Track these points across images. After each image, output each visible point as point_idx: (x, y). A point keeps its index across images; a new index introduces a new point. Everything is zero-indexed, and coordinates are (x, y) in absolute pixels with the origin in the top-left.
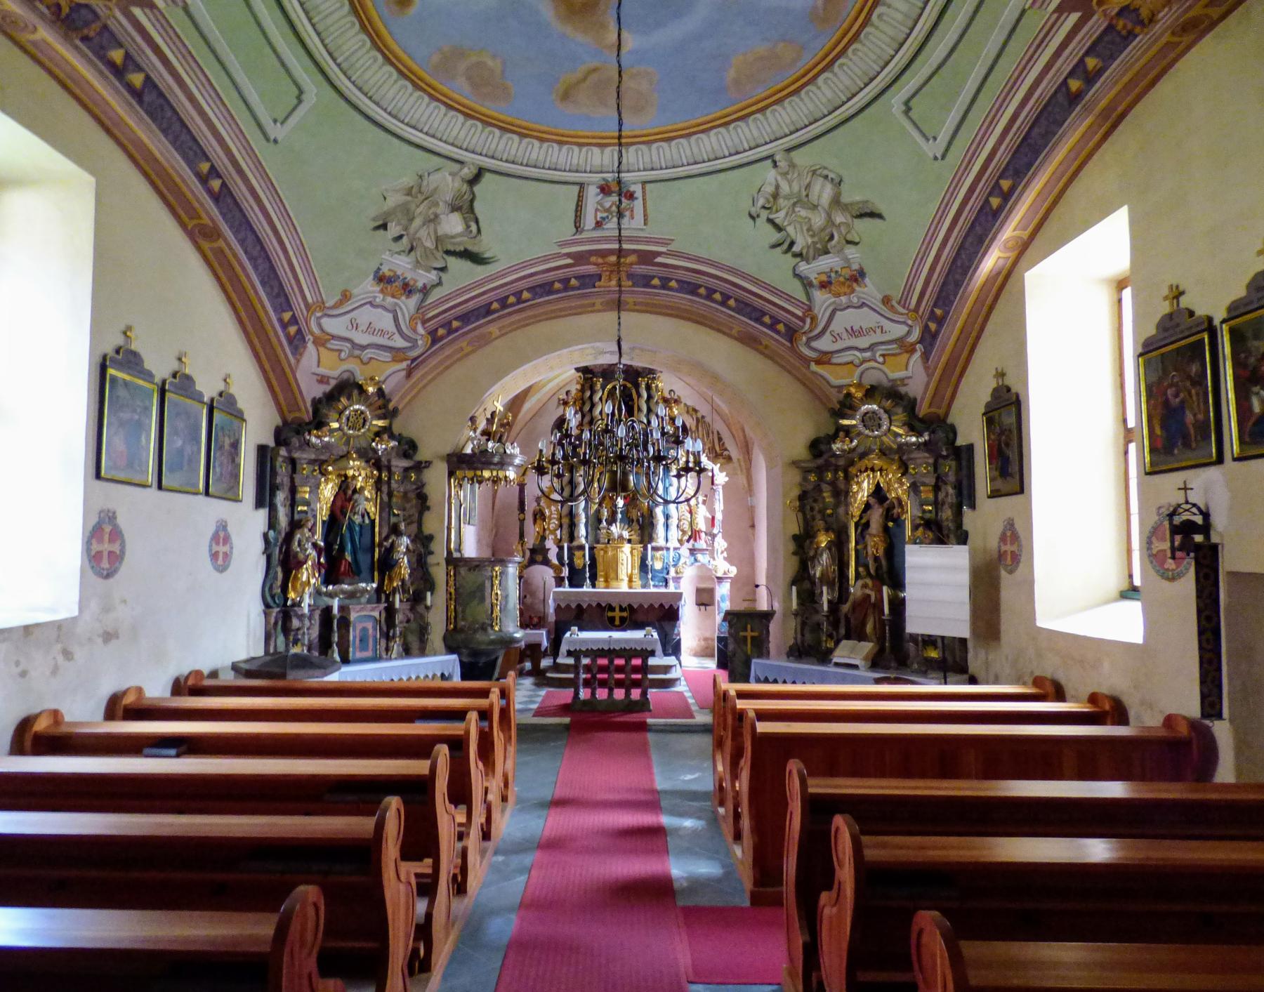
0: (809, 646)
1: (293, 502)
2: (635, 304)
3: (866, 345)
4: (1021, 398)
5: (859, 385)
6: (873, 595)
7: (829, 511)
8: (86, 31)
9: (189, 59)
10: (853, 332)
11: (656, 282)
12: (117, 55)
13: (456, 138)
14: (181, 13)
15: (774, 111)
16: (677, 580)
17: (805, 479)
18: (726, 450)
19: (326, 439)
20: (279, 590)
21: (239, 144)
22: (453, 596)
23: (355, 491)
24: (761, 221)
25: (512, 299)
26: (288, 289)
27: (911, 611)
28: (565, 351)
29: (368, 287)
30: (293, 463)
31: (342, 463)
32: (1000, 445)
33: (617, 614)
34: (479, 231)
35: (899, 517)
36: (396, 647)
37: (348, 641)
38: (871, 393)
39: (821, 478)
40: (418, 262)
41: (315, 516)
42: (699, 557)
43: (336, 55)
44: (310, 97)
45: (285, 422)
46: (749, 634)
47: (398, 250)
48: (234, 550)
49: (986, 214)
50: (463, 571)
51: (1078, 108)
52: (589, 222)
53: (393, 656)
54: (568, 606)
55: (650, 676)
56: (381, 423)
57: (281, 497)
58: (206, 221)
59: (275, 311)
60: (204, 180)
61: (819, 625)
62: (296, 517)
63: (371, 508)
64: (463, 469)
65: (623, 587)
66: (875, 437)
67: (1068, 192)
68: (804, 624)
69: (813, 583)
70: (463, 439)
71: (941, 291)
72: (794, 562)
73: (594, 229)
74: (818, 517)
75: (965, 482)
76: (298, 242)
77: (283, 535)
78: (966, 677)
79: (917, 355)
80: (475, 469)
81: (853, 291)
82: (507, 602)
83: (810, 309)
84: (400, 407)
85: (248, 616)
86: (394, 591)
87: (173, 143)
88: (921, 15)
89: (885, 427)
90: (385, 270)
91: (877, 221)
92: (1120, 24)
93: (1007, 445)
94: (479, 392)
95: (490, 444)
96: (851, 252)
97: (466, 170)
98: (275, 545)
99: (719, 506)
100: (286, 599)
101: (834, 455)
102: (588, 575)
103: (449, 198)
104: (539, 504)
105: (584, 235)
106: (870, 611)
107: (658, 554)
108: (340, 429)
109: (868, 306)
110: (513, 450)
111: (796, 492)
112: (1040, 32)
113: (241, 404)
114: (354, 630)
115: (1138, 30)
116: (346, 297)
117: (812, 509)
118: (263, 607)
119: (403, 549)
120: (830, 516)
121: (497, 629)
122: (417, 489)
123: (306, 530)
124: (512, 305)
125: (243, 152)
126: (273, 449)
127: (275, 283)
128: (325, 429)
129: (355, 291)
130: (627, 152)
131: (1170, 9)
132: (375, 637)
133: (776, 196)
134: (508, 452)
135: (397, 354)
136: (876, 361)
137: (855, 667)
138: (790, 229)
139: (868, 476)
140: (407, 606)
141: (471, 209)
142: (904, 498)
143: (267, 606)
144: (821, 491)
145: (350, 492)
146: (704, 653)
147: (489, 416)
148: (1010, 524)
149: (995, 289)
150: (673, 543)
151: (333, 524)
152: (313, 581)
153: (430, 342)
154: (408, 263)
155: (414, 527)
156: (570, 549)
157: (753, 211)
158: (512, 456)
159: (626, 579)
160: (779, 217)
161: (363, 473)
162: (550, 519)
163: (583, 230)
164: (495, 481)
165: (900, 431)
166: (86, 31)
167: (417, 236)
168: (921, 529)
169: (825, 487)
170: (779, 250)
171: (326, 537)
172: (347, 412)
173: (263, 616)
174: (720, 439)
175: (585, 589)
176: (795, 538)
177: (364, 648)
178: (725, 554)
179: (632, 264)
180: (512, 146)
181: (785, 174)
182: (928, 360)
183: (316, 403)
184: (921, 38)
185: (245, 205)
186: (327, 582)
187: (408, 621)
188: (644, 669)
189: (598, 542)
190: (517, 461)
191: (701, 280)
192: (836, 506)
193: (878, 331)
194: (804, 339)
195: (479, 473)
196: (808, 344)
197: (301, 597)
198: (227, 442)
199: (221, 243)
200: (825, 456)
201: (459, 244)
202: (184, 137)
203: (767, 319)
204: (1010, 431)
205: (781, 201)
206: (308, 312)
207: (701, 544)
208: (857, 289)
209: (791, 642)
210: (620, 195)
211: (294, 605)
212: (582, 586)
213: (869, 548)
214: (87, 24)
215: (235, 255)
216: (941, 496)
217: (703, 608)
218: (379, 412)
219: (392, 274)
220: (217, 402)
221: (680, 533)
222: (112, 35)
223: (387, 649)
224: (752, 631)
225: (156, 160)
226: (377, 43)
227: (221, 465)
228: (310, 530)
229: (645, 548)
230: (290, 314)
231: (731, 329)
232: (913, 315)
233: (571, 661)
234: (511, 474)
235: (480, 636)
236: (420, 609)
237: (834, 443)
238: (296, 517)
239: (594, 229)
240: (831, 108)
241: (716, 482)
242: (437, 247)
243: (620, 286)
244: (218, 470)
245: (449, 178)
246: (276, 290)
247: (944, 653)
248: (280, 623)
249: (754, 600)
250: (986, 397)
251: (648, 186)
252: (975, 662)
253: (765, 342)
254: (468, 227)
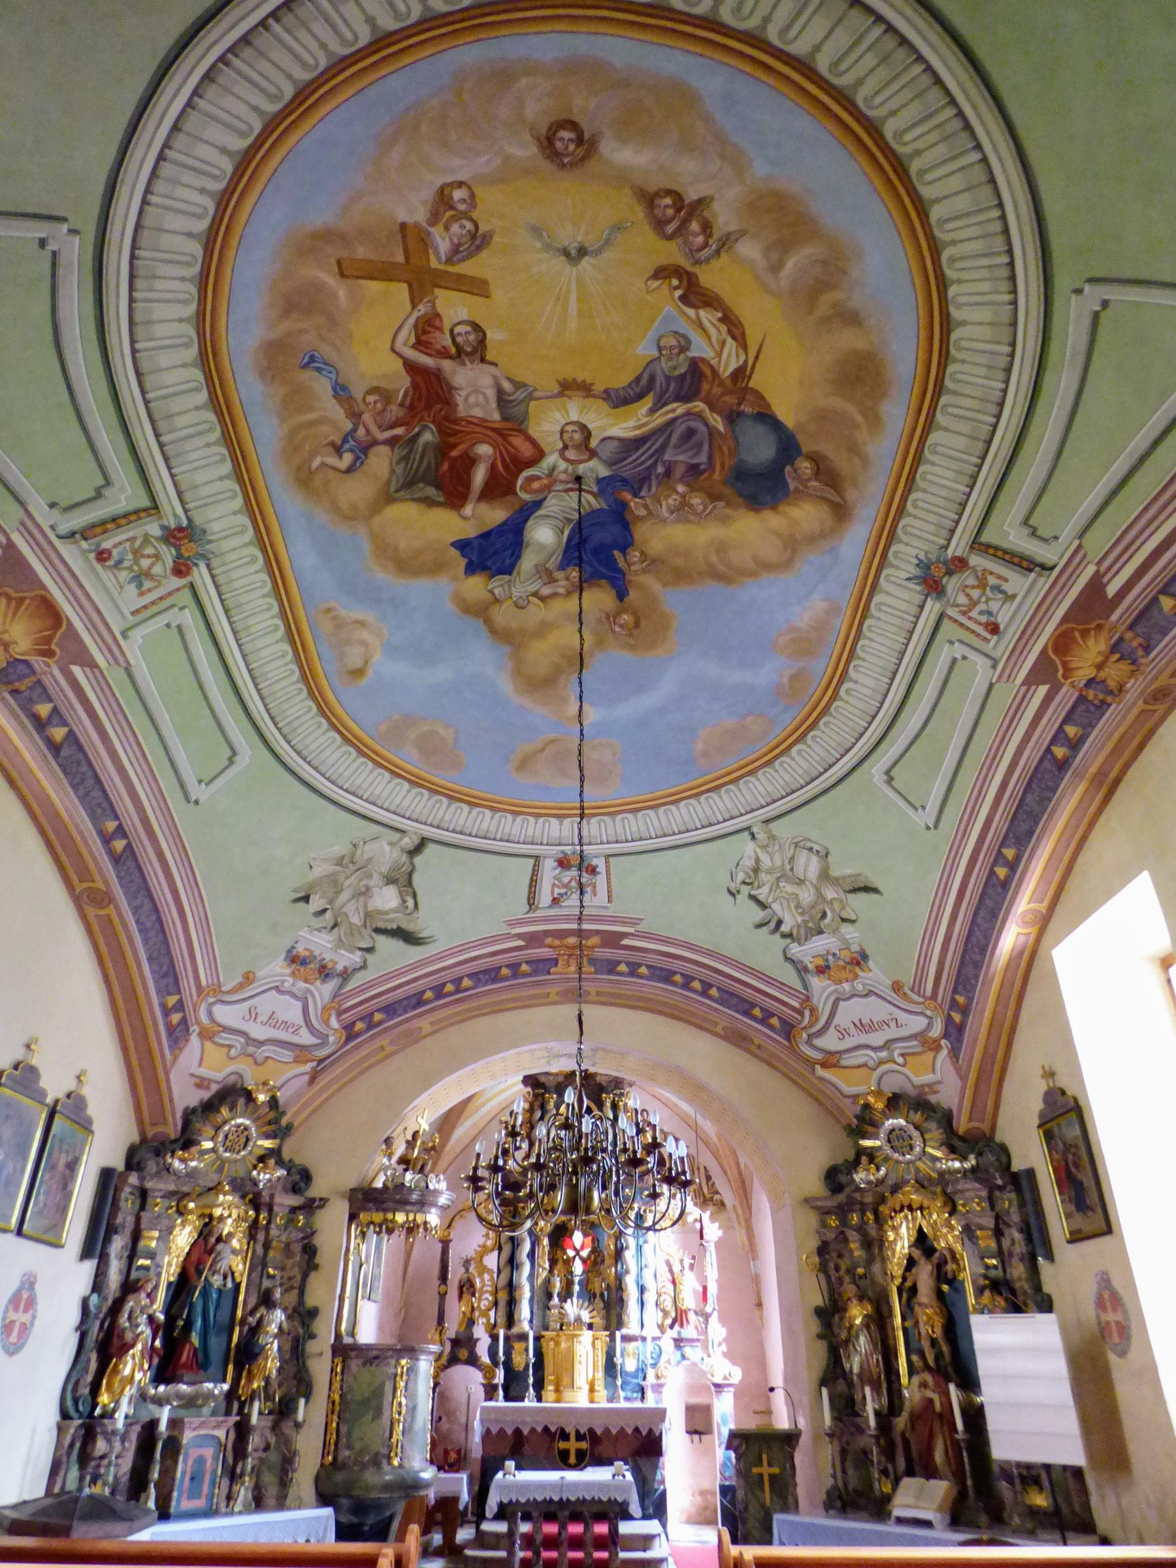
0: (855, 1491)
1: (132, 1254)
2: (598, 993)
3: (881, 1043)
4: (1082, 1102)
5: (878, 1093)
6: (936, 1397)
7: (860, 1271)
8: (17, 685)
9: (121, 717)
10: (861, 1027)
11: (622, 968)
12: (44, 710)
13: (398, 806)
14: (122, 671)
15: (746, 783)
16: (658, 1388)
17: (824, 1225)
18: (717, 1192)
19: (193, 1164)
20: (87, 1391)
21: (154, 802)
22: (337, 1408)
23: (219, 1239)
24: (742, 897)
25: (449, 988)
26: (179, 966)
27: (994, 1422)
28: (512, 1052)
29: (278, 968)
30: (143, 1195)
31: (207, 1199)
32: (1067, 1164)
33: (572, 1445)
34: (416, 906)
35: (955, 1278)
36: (243, 1493)
37: (173, 1479)
38: (894, 1102)
39: (844, 1222)
40: (340, 940)
41: (159, 1275)
42: (688, 1350)
43: (278, 719)
44: (243, 760)
45: (144, 1140)
46: (765, 1470)
47: (316, 926)
48: (37, 1322)
49: (994, 886)
50: (355, 1364)
51: (1070, 773)
52: (545, 898)
53: (236, 1509)
54: (502, 1431)
55: (623, 1555)
56: (268, 1144)
57: (118, 1244)
58: (100, 885)
59: (158, 992)
60: (107, 840)
61: (865, 1453)
62: (134, 1275)
63: (239, 1266)
64: (369, 1210)
65: (579, 1399)
66: (908, 1163)
67: (1081, 860)
68: (844, 1452)
69: (850, 1385)
70: (375, 1167)
71: (959, 974)
72: (822, 1347)
73: (550, 907)
74: (847, 1279)
75: (1033, 1222)
76: (202, 914)
77: (110, 1302)
78: (1095, 1538)
79: (944, 1053)
80: (385, 1210)
81: (856, 976)
82: (413, 1418)
83: (808, 999)
84: (296, 1124)
85: (34, 1430)
86: (253, 1397)
87: (82, 799)
88: (889, 690)
89: (918, 1149)
90: (300, 949)
91: (873, 896)
92: (1091, 694)
93: (1076, 1165)
94: (399, 1104)
95: (409, 1176)
96: (847, 930)
97: (406, 840)
98: (96, 1317)
99: (712, 1274)
100: (94, 1405)
101: (858, 1189)
102: (531, 1380)
103: (384, 869)
104: (467, 1270)
105: (539, 913)
106: (937, 1427)
107: (631, 1347)
108: (213, 1150)
109: (877, 995)
110: (439, 1184)
111: (813, 1243)
112: (1014, 700)
113: (92, 1110)
114: (185, 1461)
115: (1109, 699)
116: (248, 979)
117: (837, 1268)
118: (58, 1418)
119: (273, 1329)
120: (864, 1276)
121: (396, 1462)
122: (304, 1238)
123: (143, 1295)
124: (450, 994)
125: (158, 812)
126: (121, 1174)
127: (166, 961)
128: (194, 1149)
129: (260, 974)
130: (588, 823)
131: (1137, 680)
132: (215, 1471)
133: (756, 870)
134: (431, 1187)
135: (301, 1052)
136: (895, 1062)
137: (927, 1524)
138: (776, 907)
139: (906, 1217)
140: (268, 1421)
141: (410, 883)
142: (958, 1247)
143: (65, 1415)
144: (846, 1241)
145: (212, 1240)
146: (702, 1518)
147: (410, 1138)
148: (1105, 1281)
149: (1021, 971)
150: (651, 1331)
151: (182, 1287)
152: (138, 1376)
153: (343, 1038)
154: (329, 942)
155: (293, 1295)
156: (507, 1339)
157: (733, 886)
158: (437, 1192)
159: (586, 1387)
160: (763, 893)
161: (234, 1215)
162: (482, 1292)
163: (537, 908)
164: (411, 1229)
165: (939, 1154)
166: (17, 685)
167: (344, 910)
168: (987, 1293)
169: (853, 1236)
170: (765, 929)
171: (168, 1310)
172: (226, 1128)
173: (55, 1433)
174: (708, 1178)
175: (526, 1403)
176: (819, 1312)
177: (194, 1494)
178: (724, 1348)
179: (593, 947)
180: (461, 815)
181: (764, 847)
182: (958, 1060)
183: (189, 1116)
184: (893, 711)
185: (148, 869)
186: (158, 1379)
187: (267, 1448)
188: (612, 1541)
189: (546, 1328)
190: (443, 1200)
191: (676, 965)
192: (869, 1262)
193: (893, 1024)
194: (805, 1036)
195: (390, 1216)
196: (809, 1042)
197: (117, 1402)
198: (63, 1160)
199: (111, 910)
200: (847, 1190)
201: (392, 920)
202: (96, 793)
203: (757, 1012)
204: (1077, 1146)
205: (763, 876)
206: (199, 995)
207: (689, 1332)
208: (861, 974)
209: (830, 1482)
210: (580, 870)
211: (103, 1416)
212: (522, 1400)
213: (921, 1325)
214: (21, 678)
215: (125, 926)
216: (1006, 1243)
217: (696, 1437)
218: (266, 1129)
219: (307, 954)
220: (63, 1105)
221: (661, 1314)
222: (45, 689)
223: (229, 1497)
224: (770, 1465)
225: (57, 815)
226: (324, 709)
227: (47, 1193)
228: (149, 1296)
229: (612, 1337)
230: (177, 997)
231: (716, 1024)
232: (933, 1004)
233: (502, 1527)
234: (433, 1218)
235: (371, 1477)
236: (287, 1427)
237: (857, 1172)
238: (134, 1275)
239: (550, 907)
240: (808, 779)
241: (705, 1237)
242: (365, 925)
243: (580, 974)
244: (41, 1197)
245: (387, 848)
246: (165, 968)
247: (1055, 1500)
248: (78, 1445)
249: (768, 1412)
250: (1038, 1105)
251: (612, 860)
252: (1103, 1508)
253: (756, 1041)
254: (404, 901)
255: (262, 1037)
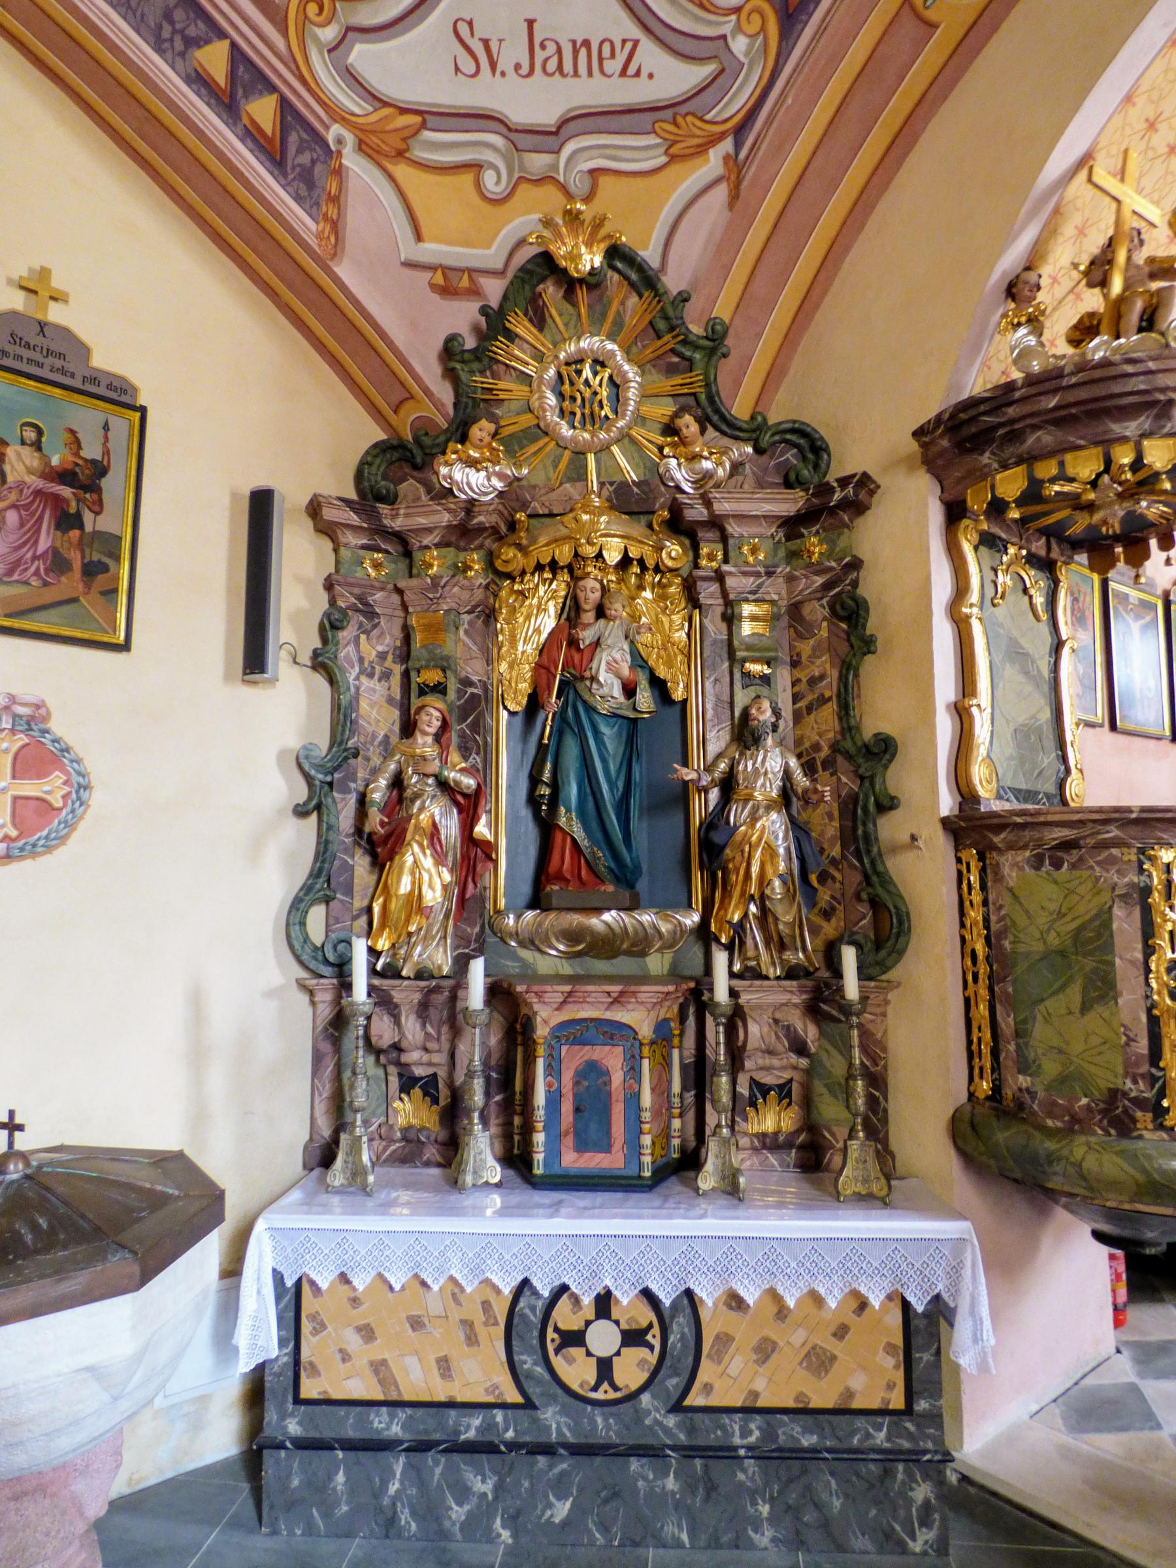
122: (827, 586)
206: (285, 33)
255: (548, 117)
